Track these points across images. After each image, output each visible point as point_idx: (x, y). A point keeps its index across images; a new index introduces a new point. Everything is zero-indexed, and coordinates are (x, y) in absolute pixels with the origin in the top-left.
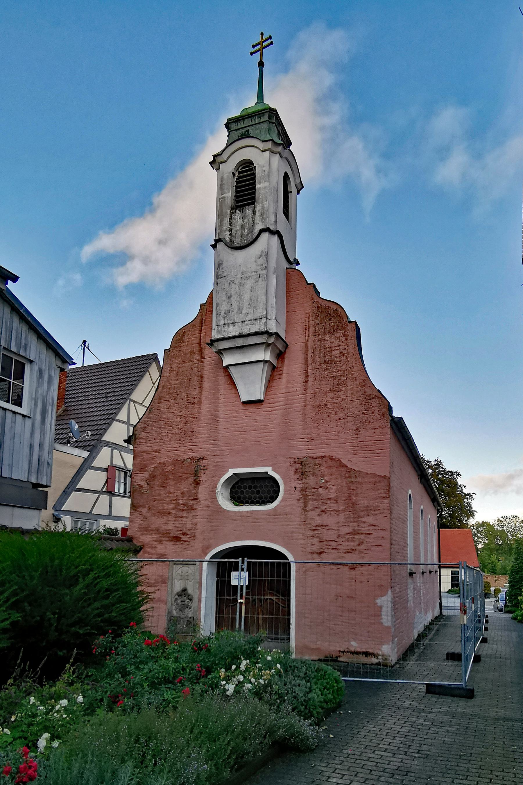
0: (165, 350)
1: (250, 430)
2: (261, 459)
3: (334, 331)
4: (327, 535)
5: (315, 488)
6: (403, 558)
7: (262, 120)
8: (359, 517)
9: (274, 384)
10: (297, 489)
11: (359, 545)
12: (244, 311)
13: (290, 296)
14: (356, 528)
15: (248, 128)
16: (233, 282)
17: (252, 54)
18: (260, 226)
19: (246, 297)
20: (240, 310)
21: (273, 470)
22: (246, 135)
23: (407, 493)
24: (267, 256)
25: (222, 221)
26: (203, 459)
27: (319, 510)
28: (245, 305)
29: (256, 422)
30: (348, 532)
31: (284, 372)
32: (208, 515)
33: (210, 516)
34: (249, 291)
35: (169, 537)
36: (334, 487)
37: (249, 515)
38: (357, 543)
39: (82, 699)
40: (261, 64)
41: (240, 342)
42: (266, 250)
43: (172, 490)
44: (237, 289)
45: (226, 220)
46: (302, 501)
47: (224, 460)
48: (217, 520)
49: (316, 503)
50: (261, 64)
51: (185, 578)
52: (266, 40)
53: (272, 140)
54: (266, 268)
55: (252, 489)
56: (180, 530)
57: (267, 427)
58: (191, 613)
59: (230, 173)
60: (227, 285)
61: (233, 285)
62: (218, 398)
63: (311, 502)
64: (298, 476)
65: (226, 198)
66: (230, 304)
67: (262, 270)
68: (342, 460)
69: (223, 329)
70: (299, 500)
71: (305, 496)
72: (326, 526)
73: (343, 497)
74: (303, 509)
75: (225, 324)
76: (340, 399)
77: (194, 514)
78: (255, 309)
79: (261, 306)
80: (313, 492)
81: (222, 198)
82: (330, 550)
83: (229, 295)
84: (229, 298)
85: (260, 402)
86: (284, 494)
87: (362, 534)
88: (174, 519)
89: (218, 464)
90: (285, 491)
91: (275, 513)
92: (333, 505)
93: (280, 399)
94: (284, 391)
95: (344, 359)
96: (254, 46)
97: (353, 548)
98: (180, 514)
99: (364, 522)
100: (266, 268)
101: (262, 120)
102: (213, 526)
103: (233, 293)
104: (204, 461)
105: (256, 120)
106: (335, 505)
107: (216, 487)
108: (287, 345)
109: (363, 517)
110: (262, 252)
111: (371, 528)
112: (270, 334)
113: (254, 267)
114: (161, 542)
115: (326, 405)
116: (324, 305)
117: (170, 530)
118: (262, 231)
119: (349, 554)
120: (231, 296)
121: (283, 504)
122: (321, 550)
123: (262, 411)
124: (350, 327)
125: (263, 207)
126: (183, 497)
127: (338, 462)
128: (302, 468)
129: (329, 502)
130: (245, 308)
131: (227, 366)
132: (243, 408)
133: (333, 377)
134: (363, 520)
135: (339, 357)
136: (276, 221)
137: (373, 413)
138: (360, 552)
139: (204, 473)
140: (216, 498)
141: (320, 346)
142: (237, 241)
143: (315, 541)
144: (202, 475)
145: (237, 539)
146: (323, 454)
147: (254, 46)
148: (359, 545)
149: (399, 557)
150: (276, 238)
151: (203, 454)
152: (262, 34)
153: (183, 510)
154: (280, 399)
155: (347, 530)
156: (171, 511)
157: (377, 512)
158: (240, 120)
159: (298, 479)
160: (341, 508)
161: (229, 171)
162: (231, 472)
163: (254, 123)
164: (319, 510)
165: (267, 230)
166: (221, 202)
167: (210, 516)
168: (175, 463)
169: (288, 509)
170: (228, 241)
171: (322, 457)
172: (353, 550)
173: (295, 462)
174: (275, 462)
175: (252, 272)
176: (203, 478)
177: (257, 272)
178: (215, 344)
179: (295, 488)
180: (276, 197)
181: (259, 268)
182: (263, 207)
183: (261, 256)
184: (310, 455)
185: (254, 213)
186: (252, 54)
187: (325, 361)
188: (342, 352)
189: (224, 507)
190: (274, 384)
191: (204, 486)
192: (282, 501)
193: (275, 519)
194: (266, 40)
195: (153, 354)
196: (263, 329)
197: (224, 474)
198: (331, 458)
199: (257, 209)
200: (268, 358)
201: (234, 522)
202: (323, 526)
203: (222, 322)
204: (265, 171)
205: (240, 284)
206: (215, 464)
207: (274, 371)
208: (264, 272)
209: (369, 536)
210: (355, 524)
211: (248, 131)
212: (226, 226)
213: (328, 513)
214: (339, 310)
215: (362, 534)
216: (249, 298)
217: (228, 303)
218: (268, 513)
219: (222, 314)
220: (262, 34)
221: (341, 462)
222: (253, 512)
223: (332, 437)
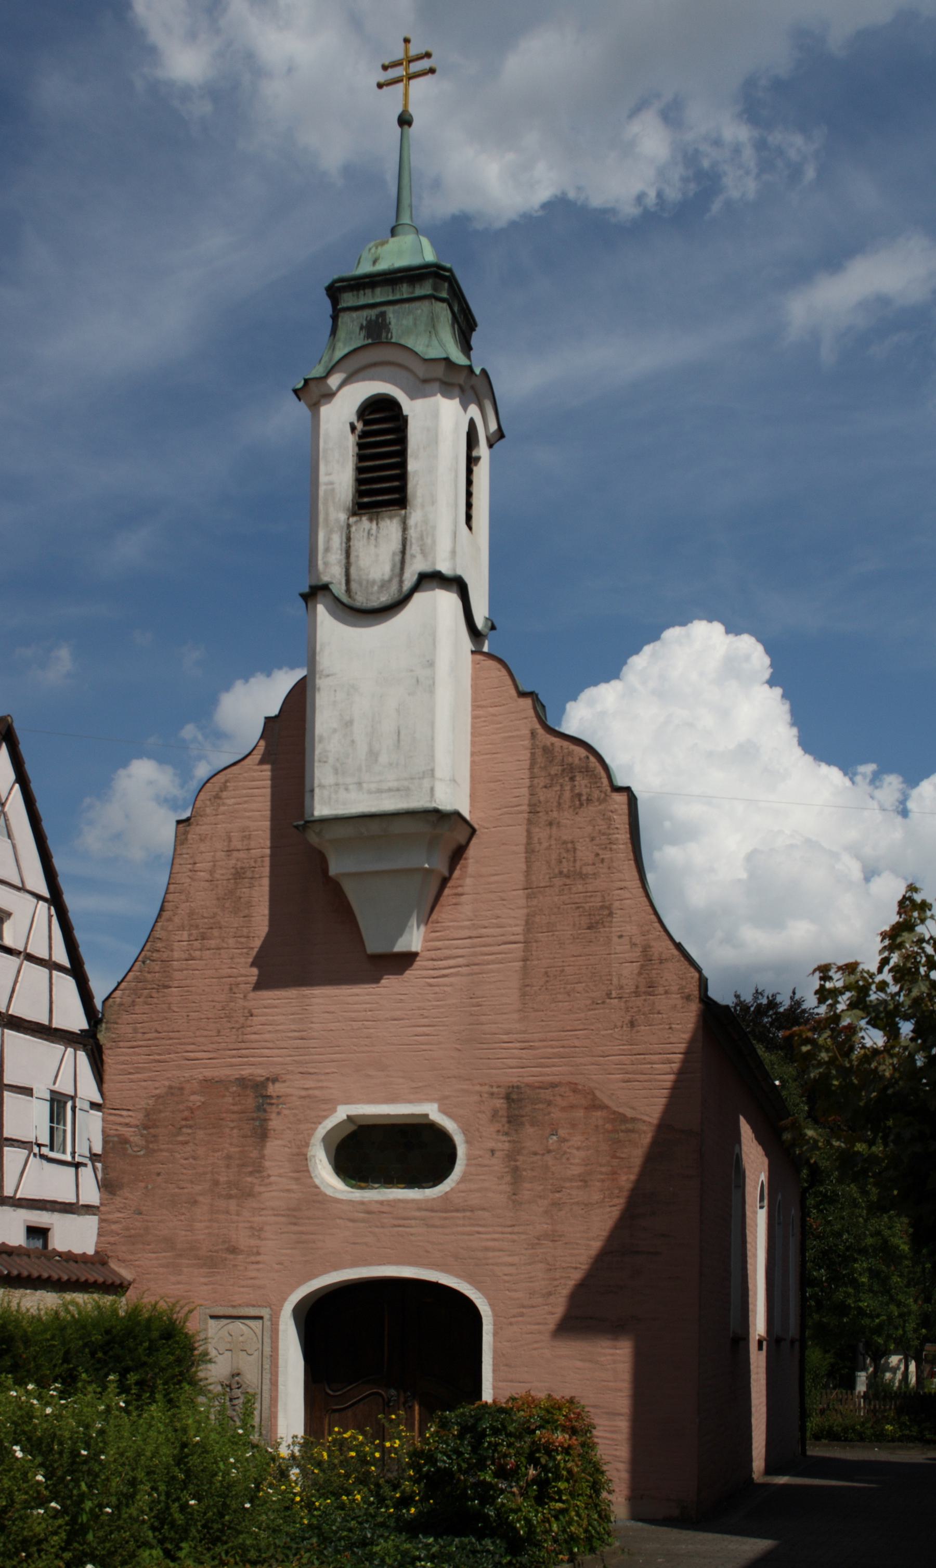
1: (387, 1020)
5: (535, 1154)
10: (497, 1154)
15: (383, 309)
17: (380, 86)
18: (416, 566)
21: (442, 1111)
23: (759, 1178)
27: (546, 1202)
29: (401, 1001)
31: (466, 889)
33: (294, 1210)
37: (385, 1208)
39: (868, 1043)
47: (325, 1084)
48: (309, 1218)
52: (419, 58)
57: (425, 1013)
68: (597, 1093)
69: (333, 796)
71: (515, 1171)
75: (337, 785)
80: (533, 1163)
83: (348, 718)
86: (467, 1165)
89: (311, 1092)
90: (469, 1158)
91: (446, 1205)
102: (302, 1233)
104: (277, 1085)
105: (405, 291)
121: (462, 1187)
128: (516, 1107)
139: (279, 1113)
140: (308, 1171)
141: (550, 837)
142: (361, 600)
144: (273, 1116)
145: (354, 1264)
146: (556, 1079)
147: (385, 68)
151: (277, 1070)
153: (230, 1197)
162: (342, 1113)
163: (398, 297)
164: (546, 1202)
167: (294, 1210)
171: (553, 1085)
173: (492, 1094)
174: (447, 1093)
176: (275, 1123)
177: (412, 671)
186: (380, 86)
187: (561, 873)
192: (463, 1180)
193: (446, 1218)
194: (419, 58)
197: (326, 1117)
198: (575, 1088)
206: (303, 1093)
211: (383, 315)
221: (595, 1098)
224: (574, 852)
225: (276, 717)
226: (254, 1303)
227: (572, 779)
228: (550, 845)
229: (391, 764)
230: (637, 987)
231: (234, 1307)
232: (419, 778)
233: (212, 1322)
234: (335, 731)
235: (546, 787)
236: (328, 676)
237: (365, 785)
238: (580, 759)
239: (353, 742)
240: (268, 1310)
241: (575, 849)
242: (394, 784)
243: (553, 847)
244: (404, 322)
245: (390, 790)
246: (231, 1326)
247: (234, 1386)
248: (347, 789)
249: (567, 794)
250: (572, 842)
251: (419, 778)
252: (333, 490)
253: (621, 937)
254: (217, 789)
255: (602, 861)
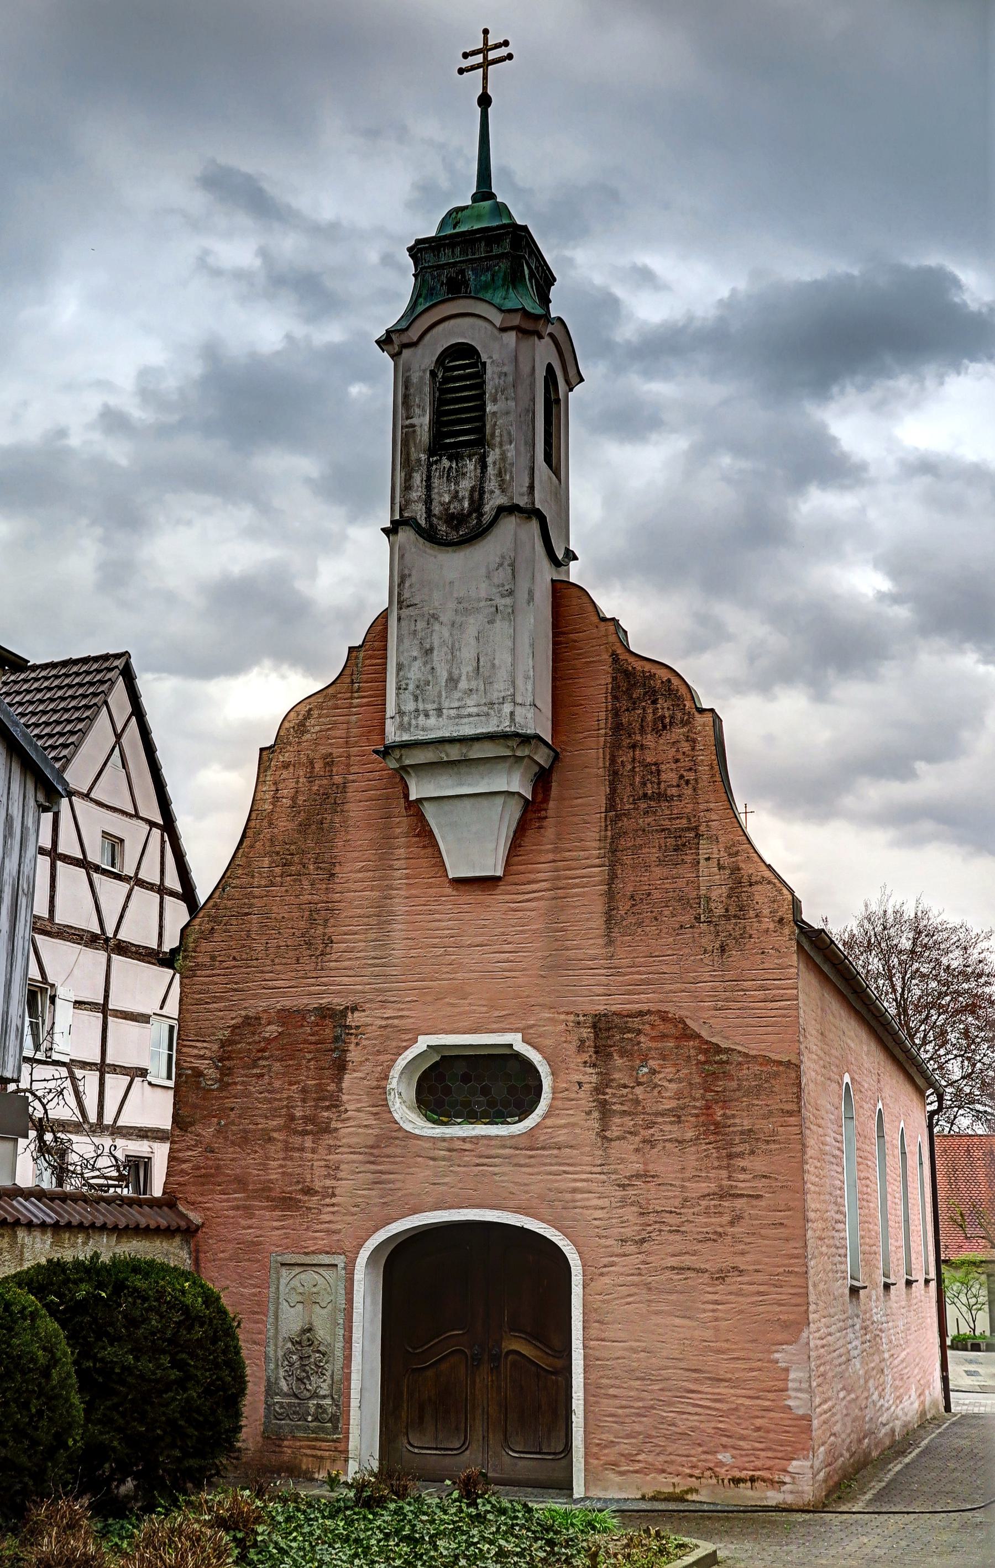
0: (262, 750)
2: (497, 1014)
3: (664, 727)
4: (657, 1198)
5: (625, 1087)
6: (834, 1250)
7: (496, 251)
8: (730, 1156)
9: (527, 841)
11: (732, 1223)
12: (463, 685)
13: (561, 643)
14: (725, 1183)
16: (435, 617)
17: (461, 71)
19: (467, 653)
20: (453, 681)
22: (456, 288)
24: (512, 565)
25: (408, 478)
26: (354, 1009)
28: (464, 672)
30: (706, 1191)
31: (550, 813)
32: (366, 1147)
33: (372, 1147)
34: (473, 642)
35: (268, 1199)
36: (673, 1086)
37: (467, 1146)
38: (726, 1219)
40: (485, 101)
41: (454, 753)
42: (512, 555)
43: (277, 1084)
44: (446, 634)
45: (417, 478)
46: (596, 1114)
49: (628, 1122)
50: (485, 101)
51: (309, 1300)
53: (523, 309)
54: (511, 593)
55: (474, 1085)
56: (298, 1182)
58: (325, 1386)
59: (424, 371)
60: (421, 625)
61: (437, 627)
62: (391, 868)
63: (617, 1120)
64: (585, 1057)
65: (418, 429)
66: (429, 667)
67: (503, 596)
68: (688, 1021)
69: (413, 722)
70: (589, 1113)
72: (653, 1177)
73: (695, 1107)
74: (597, 1134)
75: (417, 710)
76: (681, 883)
77: (331, 1142)
78: (488, 682)
79: (502, 674)
81: (407, 427)
82: (665, 1236)
84: (429, 652)
85: (497, 879)
87: (742, 1196)
88: (281, 1155)
91: (530, 1142)
92: (667, 1128)
93: (541, 876)
94: (551, 856)
95: (688, 791)
96: (466, 55)
97: (720, 1230)
98: (296, 1140)
99: (744, 1170)
100: (511, 593)
101: (496, 251)
102: (381, 1172)
103: (436, 644)
104: (356, 1014)
106: (675, 1127)
107: (386, 1078)
108: (557, 754)
109: (741, 1155)
110: (503, 557)
111: (760, 1183)
112: (526, 739)
113: (484, 589)
114: (248, 1211)
115: (649, 894)
116: (639, 668)
117: (271, 1181)
118: (503, 511)
119: (710, 1244)
120: (431, 650)
122: (644, 1234)
123: (499, 899)
124: (699, 719)
125: (503, 457)
126: (304, 1100)
127: (681, 1026)
129: (660, 1120)
130: (464, 678)
131: (420, 801)
132: (449, 891)
133: (663, 830)
134: (742, 1163)
135: (678, 786)
136: (531, 488)
137: (757, 916)
138: (736, 1240)
139: (357, 1044)
141: (634, 759)
143: (630, 1213)
144: (352, 1047)
146: (645, 1007)
147: (466, 55)
148: (732, 1223)
149: (824, 1249)
150: (535, 525)
152: (486, 32)
154: (541, 876)
155: (705, 1187)
156: (275, 1135)
157: (773, 1146)
158: (444, 246)
159: (585, 1062)
160: (690, 1134)
161: (423, 367)
162: (423, 1042)
165: (512, 509)
166: (404, 439)
167: (372, 1147)
168: (287, 1016)
169: (562, 1136)
170: (423, 523)
171: (641, 1014)
172: (720, 1235)
173: (579, 1023)
175: (479, 600)
176: (354, 1055)
177: (491, 600)
178: (397, 753)
179: (580, 1084)
180: (530, 434)
181: (494, 590)
182: (503, 457)
183: (501, 565)
184: (614, 1008)
185: (484, 467)
186: (461, 71)
187: (645, 795)
188: (682, 777)
189: (407, 1127)
190: (526, 840)
191: (356, 1074)
193: (531, 1157)
195: (117, 656)
196: (506, 726)
199: (490, 460)
200: (515, 788)
201: (432, 1163)
202: (646, 1176)
203: (410, 706)
204: (506, 374)
205: (453, 625)
206: (384, 1023)
207: (531, 815)
208: (508, 601)
209: (754, 1202)
210: (724, 1173)
212: (417, 493)
213: (660, 1147)
214: (675, 681)
215: (742, 1196)
216: (473, 655)
217: (425, 663)
218: (512, 1142)
219: (411, 687)
220: (486, 32)
222: (476, 1139)
223: (664, 968)
224: (659, 775)
225: (360, 646)
226: (328, 1249)
227: (655, 702)
228: (634, 767)
229: (471, 690)
230: (727, 910)
231: (306, 1254)
232: (499, 704)
233: (284, 1271)
234: (415, 659)
235: (627, 710)
236: (408, 606)
237: (444, 711)
238: (662, 682)
239: (433, 668)
240: (342, 1257)
241: (659, 772)
242: (474, 710)
243: (637, 769)
244: (483, 278)
245: (470, 715)
246: (303, 1276)
247: (305, 1343)
248: (427, 716)
249: (650, 718)
250: (656, 764)
251: (499, 704)
252: (414, 431)
253: (708, 859)
254: (300, 717)
255: (687, 782)
